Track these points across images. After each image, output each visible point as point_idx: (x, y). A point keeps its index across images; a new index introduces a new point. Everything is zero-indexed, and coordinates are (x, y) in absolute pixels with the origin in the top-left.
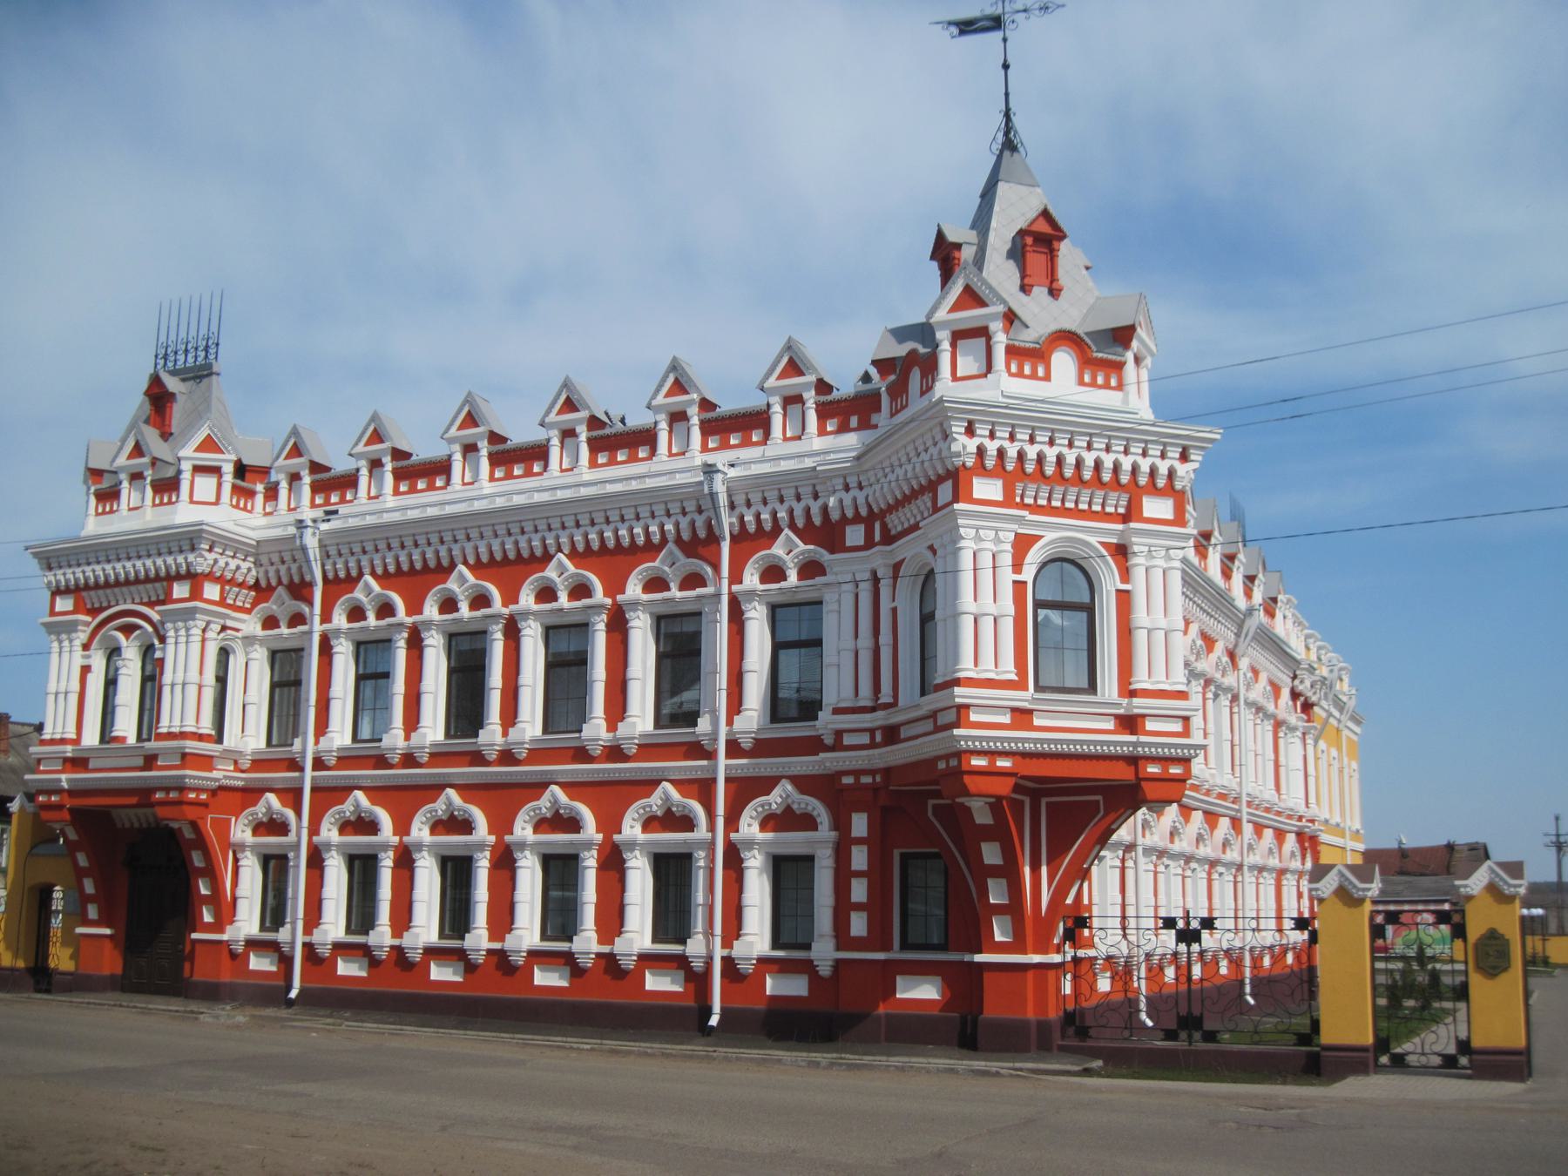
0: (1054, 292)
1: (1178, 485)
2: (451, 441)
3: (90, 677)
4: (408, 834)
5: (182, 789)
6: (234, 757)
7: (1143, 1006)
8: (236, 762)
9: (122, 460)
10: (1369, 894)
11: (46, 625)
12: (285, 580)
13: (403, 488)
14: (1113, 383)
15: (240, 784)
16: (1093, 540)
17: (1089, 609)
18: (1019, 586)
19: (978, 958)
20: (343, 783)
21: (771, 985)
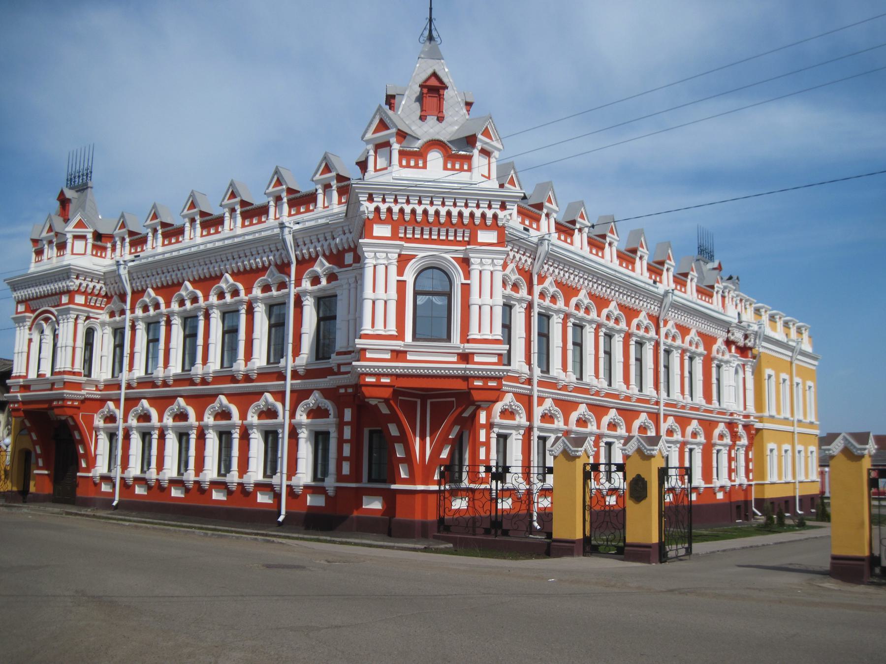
0: (440, 119)
2: (317, 182)
3: (32, 344)
4: (246, 419)
5: (64, 400)
6: (96, 384)
7: (535, 518)
10: (866, 452)
11: (14, 319)
13: (166, 243)
14: (466, 167)
15: (98, 397)
16: (448, 256)
17: (449, 295)
18: (401, 285)
19: (393, 487)
20: (258, 390)
21: (310, 500)
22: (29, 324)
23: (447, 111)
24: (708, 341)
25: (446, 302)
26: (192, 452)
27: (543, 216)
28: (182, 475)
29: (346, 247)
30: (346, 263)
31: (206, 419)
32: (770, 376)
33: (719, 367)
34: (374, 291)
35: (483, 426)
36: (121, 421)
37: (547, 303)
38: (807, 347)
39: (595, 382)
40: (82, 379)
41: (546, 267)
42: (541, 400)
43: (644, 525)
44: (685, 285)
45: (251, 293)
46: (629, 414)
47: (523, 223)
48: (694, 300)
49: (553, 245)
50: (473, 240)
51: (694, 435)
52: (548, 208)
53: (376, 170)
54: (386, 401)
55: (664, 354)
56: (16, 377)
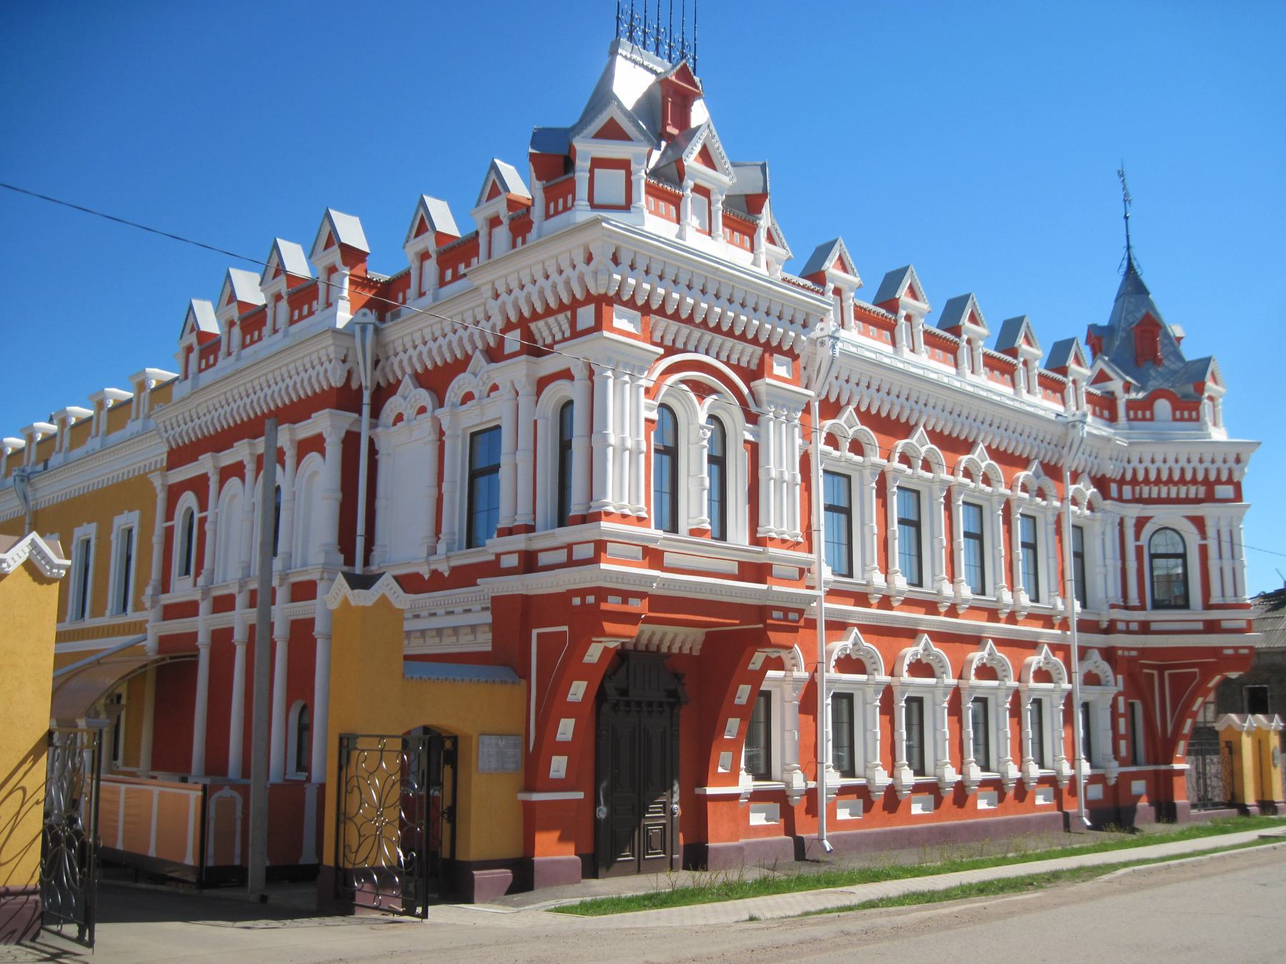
17: (1183, 556)
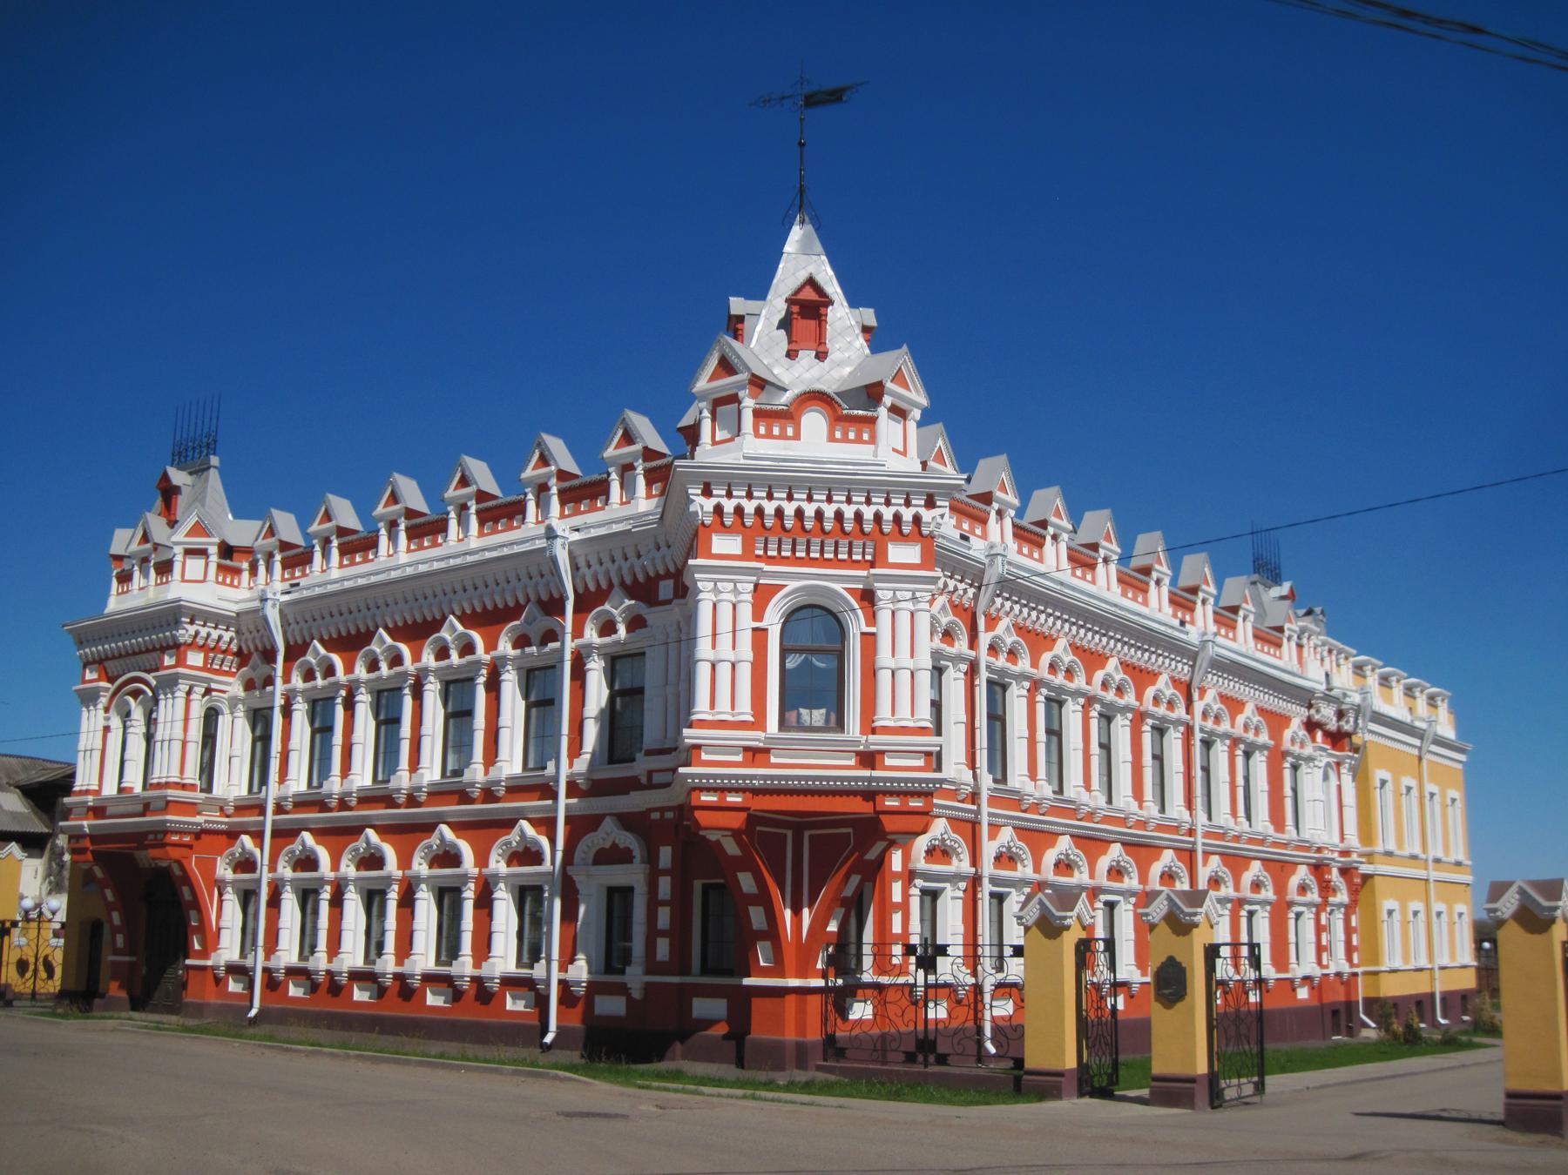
0: (821, 356)
1: (925, 531)
3: (110, 736)
5: (166, 832)
8: (222, 809)
9: (134, 547)
12: (533, 597)
16: (838, 587)
17: (840, 656)
18: (760, 635)
19: (747, 981)
22: (103, 701)
23: (834, 343)
24: (1277, 722)
25: (835, 664)
26: (391, 922)
27: (993, 515)
28: (374, 963)
29: (662, 572)
30: (662, 597)
31: (415, 866)
32: (1383, 782)
33: (1295, 768)
34: (714, 647)
35: (897, 876)
36: (265, 869)
37: (1001, 662)
38: (1447, 731)
39: (1084, 797)
40: (199, 796)
41: (999, 601)
42: (995, 829)
43: (1183, 1042)
44: (1234, 628)
45: (495, 648)
46: (1142, 850)
47: (958, 526)
48: (1250, 653)
49: (1009, 563)
50: (878, 559)
51: (1257, 886)
52: (1000, 501)
53: (714, 443)
54: (736, 834)
55: (1201, 744)
56: (81, 793)
